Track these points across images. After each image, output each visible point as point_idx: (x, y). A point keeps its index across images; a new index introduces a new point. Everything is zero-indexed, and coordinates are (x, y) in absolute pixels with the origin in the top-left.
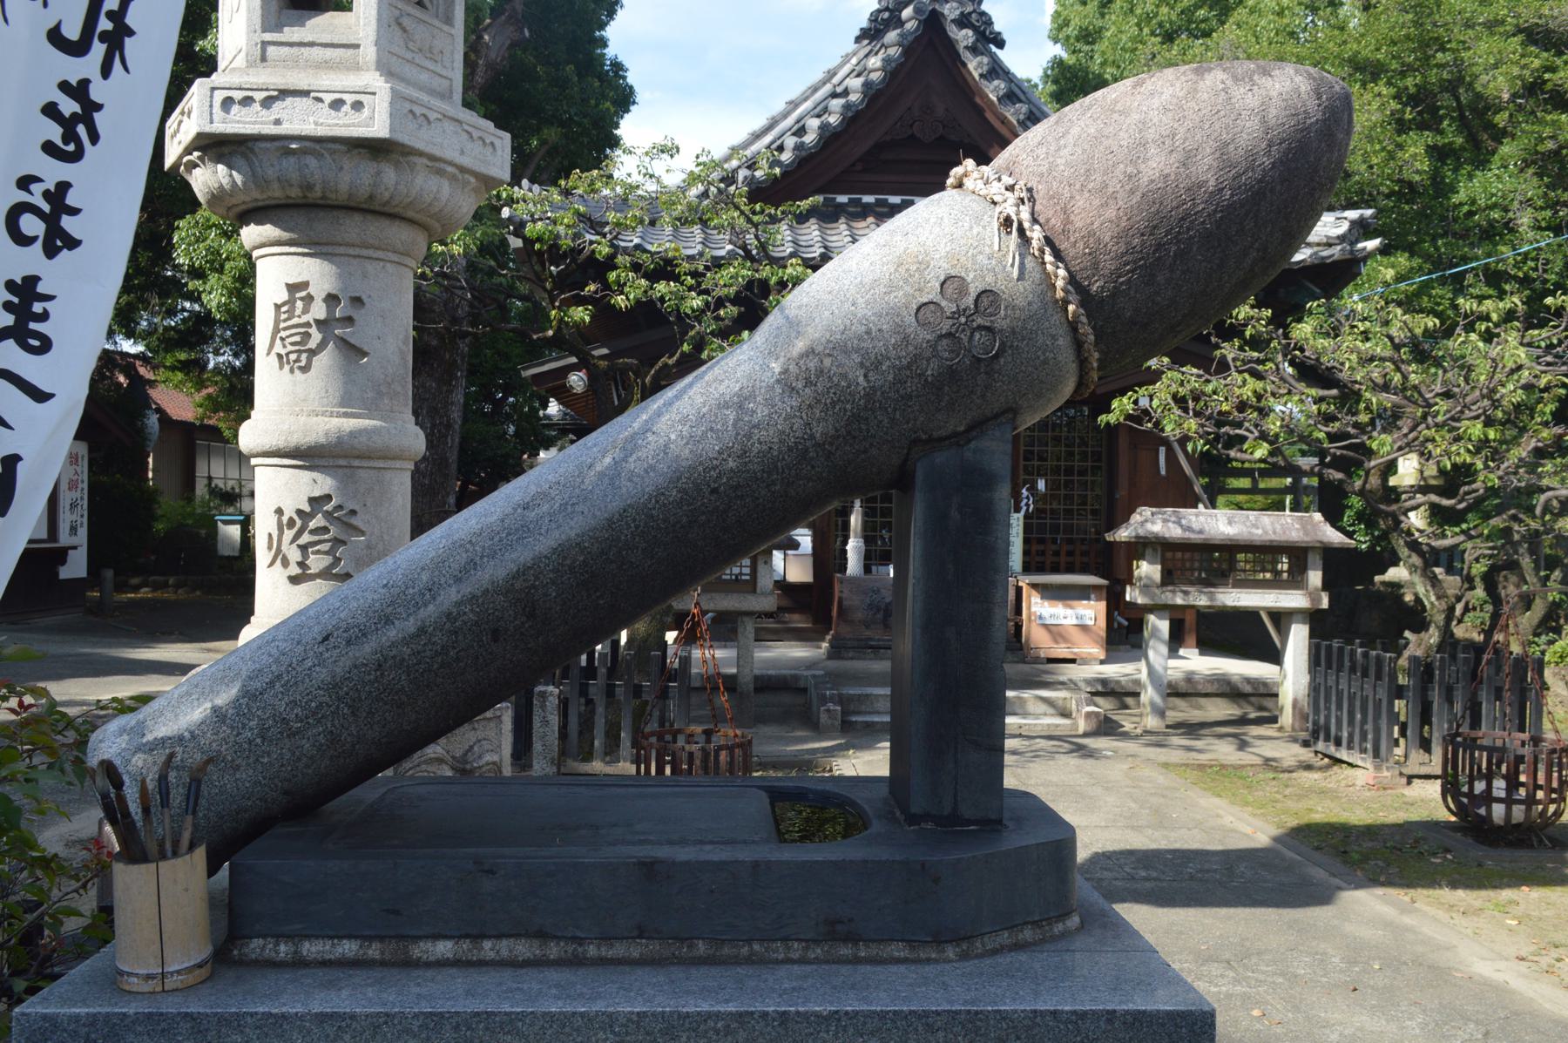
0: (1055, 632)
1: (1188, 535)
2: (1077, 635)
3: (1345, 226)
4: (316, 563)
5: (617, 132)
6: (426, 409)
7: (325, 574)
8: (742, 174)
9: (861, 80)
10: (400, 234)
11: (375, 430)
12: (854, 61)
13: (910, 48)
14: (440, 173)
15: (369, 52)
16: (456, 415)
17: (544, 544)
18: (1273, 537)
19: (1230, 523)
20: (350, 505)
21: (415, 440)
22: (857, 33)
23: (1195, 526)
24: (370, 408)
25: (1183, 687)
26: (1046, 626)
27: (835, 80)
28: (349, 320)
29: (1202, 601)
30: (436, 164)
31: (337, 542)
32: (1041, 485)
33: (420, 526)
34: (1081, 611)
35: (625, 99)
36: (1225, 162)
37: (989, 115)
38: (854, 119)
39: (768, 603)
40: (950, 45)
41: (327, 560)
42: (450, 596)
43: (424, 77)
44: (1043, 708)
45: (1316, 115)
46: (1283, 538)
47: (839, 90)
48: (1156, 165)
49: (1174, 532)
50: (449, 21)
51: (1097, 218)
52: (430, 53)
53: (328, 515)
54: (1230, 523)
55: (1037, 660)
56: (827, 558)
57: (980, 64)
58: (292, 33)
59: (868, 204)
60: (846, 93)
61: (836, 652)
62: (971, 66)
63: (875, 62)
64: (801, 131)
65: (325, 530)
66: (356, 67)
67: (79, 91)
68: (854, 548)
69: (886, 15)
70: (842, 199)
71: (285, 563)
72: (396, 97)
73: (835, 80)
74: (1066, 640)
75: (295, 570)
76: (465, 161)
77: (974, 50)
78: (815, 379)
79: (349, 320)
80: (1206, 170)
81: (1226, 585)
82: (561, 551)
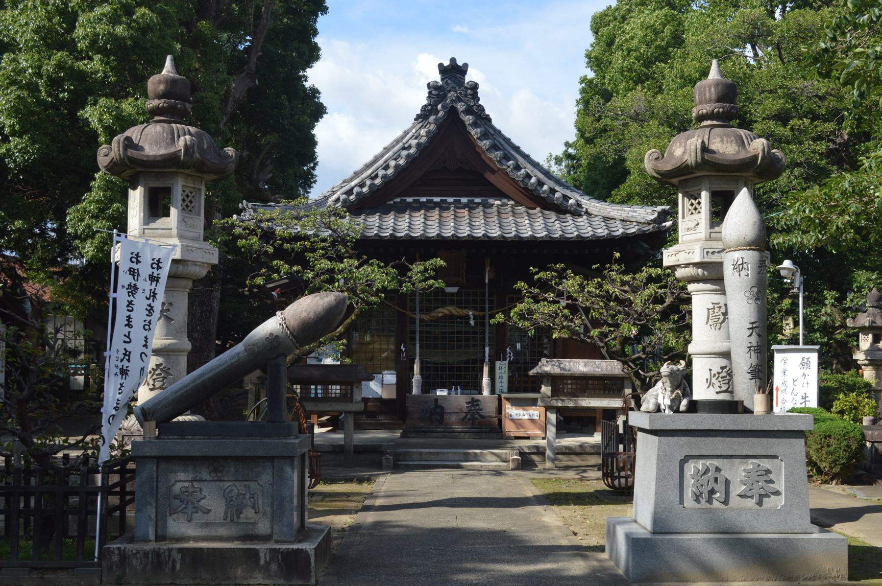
0: (517, 423)
1: (563, 372)
2: (529, 425)
3: (656, 215)
4: (158, 384)
5: (313, 132)
6: (190, 337)
7: (160, 388)
8: (356, 190)
9: (416, 141)
10: (184, 283)
11: (176, 344)
12: (414, 131)
13: (440, 125)
14: (196, 265)
15: (175, 231)
16: (216, 305)
17: (207, 377)
18: (605, 372)
19: (585, 366)
20: (168, 367)
21: (188, 346)
22: (415, 117)
23: (567, 368)
24: (174, 337)
25: (579, 450)
26: (513, 420)
27: (405, 141)
28: (168, 310)
29: (571, 404)
30: (195, 263)
31: (164, 378)
32: (519, 346)
33: (188, 373)
34: (531, 412)
35: (319, 111)
36: (315, 314)
37: (483, 157)
38: (412, 161)
39: (360, 407)
40: (462, 122)
41: (161, 383)
42: (192, 385)
43: (191, 234)
44: (495, 458)
45: (334, 302)
46: (610, 373)
47: (406, 146)
48: (304, 315)
49: (557, 371)
50: (199, 215)
51: (293, 323)
52: (193, 227)
53: (161, 370)
54: (585, 366)
55: (509, 438)
56: (403, 384)
57: (476, 132)
58: (152, 225)
59: (423, 202)
60: (410, 147)
61: (403, 436)
62: (473, 133)
63: (423, 132)
64: (386, 167)
65: (160, 374)
66: (171, 237)
67: (150, 305)
68: (417, 378)
69: (430, 108)
70: (410, 200)
71: (148, 385)
72: (183, 246)
73: (405, 141)
74: (523, 427)
75: (151, 387)
76: (204, 260)
77: (475, 125)
78: (249, 349)
79: (168, 310)
80: (312, 315)
81: (584, 396)
82: (209, 378)
